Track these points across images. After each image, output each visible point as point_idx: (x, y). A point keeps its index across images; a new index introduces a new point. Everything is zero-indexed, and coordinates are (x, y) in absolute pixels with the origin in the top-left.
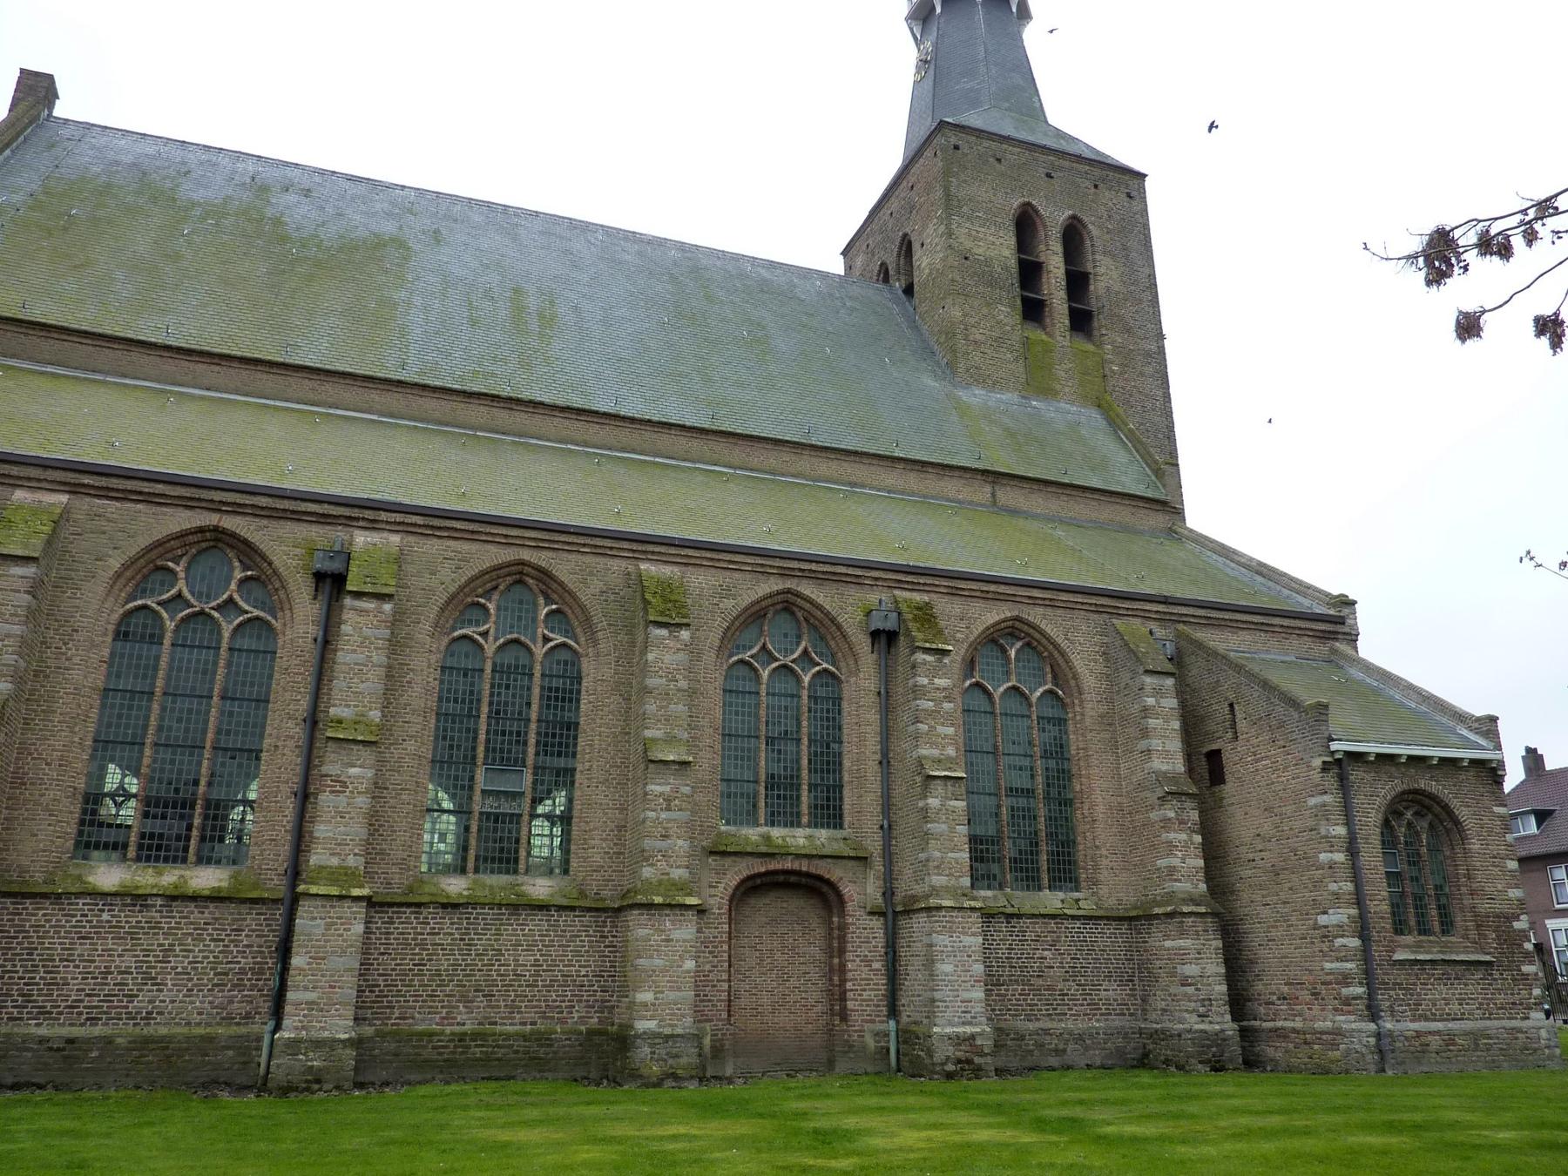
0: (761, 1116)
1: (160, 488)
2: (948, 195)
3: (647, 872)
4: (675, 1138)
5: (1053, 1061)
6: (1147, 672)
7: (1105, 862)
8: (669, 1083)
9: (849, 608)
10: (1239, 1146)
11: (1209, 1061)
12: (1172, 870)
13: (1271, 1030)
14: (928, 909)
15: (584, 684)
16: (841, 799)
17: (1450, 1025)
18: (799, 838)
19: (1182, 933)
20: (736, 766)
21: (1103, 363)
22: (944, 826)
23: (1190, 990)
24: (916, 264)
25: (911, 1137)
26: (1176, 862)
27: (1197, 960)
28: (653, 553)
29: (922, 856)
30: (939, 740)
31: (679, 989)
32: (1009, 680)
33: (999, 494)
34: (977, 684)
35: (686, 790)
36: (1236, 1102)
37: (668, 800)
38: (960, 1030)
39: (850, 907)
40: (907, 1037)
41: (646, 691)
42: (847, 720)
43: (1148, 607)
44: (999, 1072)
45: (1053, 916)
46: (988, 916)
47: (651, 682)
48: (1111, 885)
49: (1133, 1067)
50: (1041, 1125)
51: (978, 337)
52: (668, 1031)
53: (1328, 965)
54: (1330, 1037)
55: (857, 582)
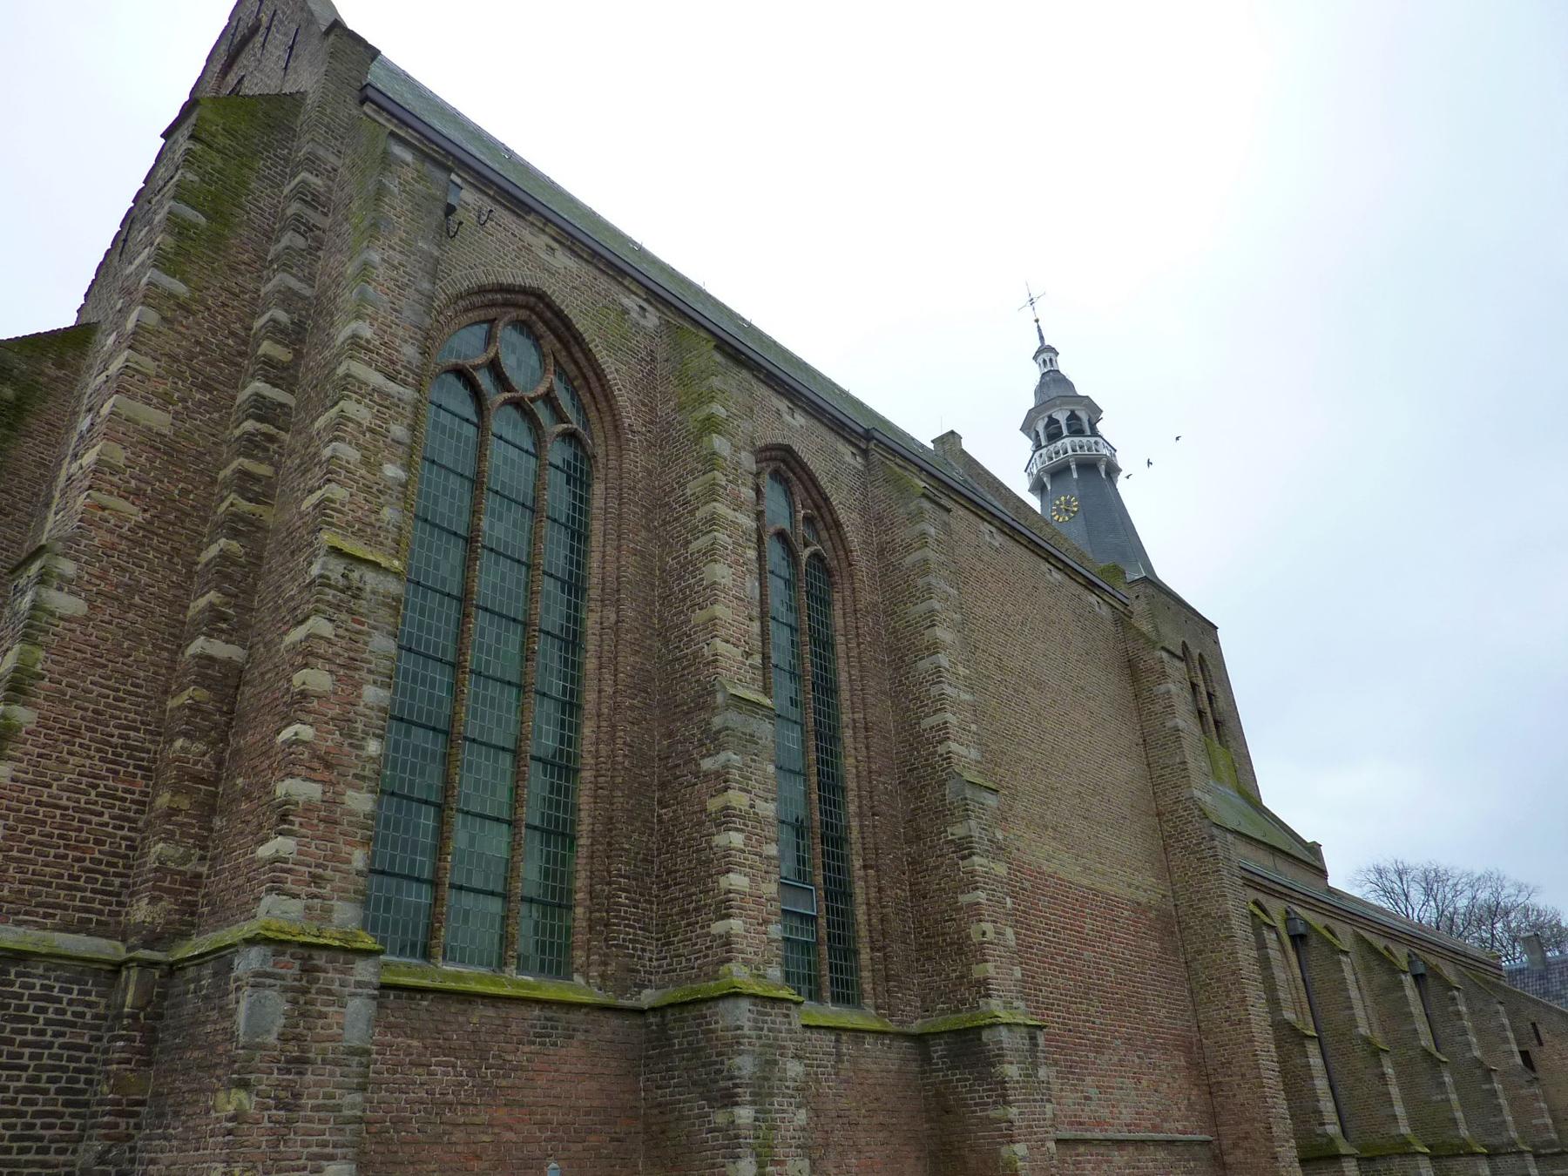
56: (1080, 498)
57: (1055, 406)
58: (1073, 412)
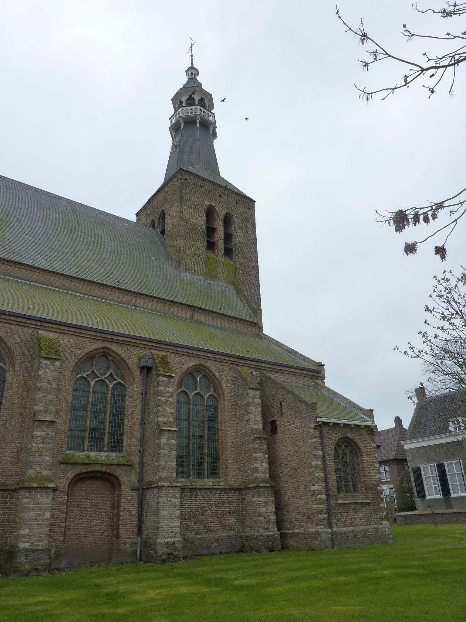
0: (80, 588)
2: (181, 196)
3: (30, 472)
4: (38, 603)
5: (206, 552)
6: (250, 388)
7: (230, 466)
8: (33, 573)
9: (132, 357)
10: (291, 586)
11: (269, 548)
12: (256, 469)
13: (291, 534)
14: (158, 487)
15: (7, 384)
16: (122, 440)
17: (357, 528)
18: (102, 456)
19: (260, 495)
20: (76, 424)
21: (236, 269)
22: (167, 451)
23: (262, 518)
24: (166, 222)
25: (152, 594)
26: (258, 466)
27: (264, 506)
28: (45, 327)
29: (157, 464)
30: (166, 414)
31: (42, 527)
32: (196, 390)
33: (195, 315)
34: (183, 391)
35: (52, 434)
36: (284, 566)
37: (43, 439)
38: (169, 540)
39: (123, 487)
40: (145, 544)
41: (37, 388)
42: (127, 405)
43: (251, 363)
44: (185, 558)
45: (209, 489)
46: (183, 489)
47: (39, 384)
48: (232, 475)
49: (238, 552)
50: (208, 582)
51: (189, 253)
52: (34, 548)
53: (314, 506)
54: (314, 535)
55: (136, 346)
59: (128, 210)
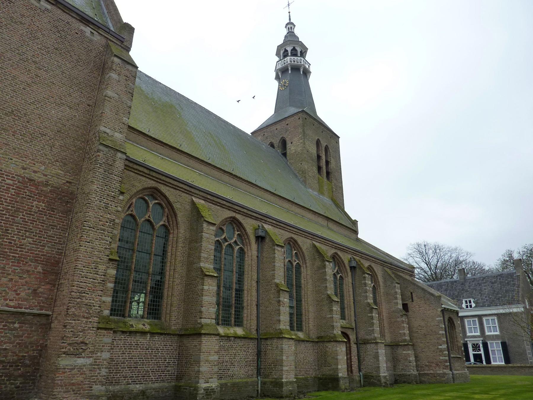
1: (224, 203)
56: (289, 82)
57: (287, 45)
58: (294, 48)
59: (249, 130)
